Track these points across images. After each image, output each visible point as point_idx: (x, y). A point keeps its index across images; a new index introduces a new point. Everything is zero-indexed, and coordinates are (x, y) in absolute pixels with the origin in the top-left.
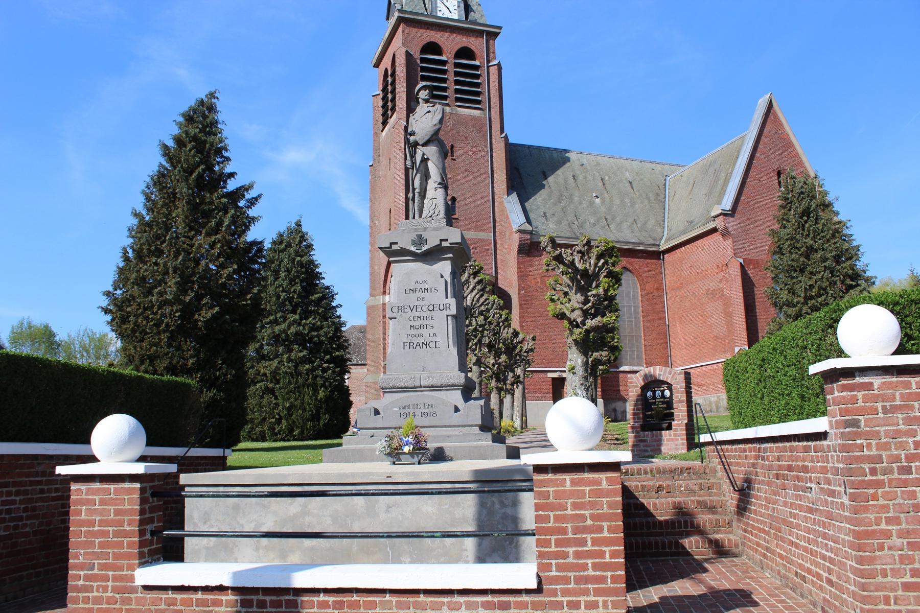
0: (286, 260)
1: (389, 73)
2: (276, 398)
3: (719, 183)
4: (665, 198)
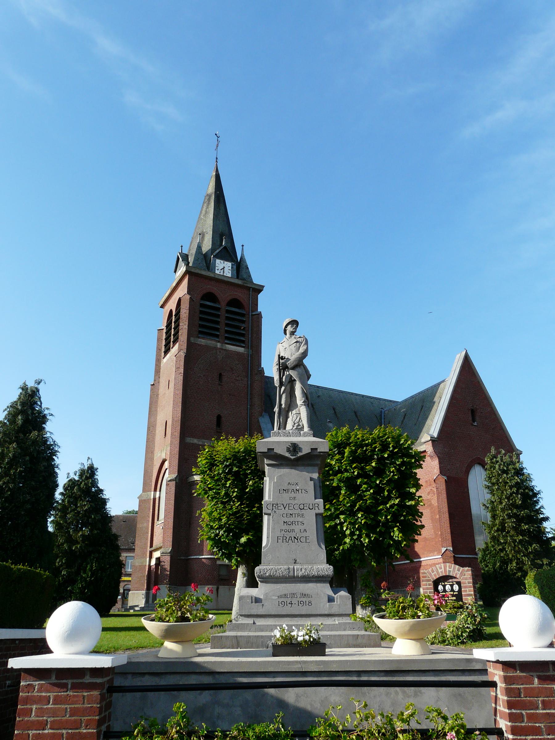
1: (174, 314)
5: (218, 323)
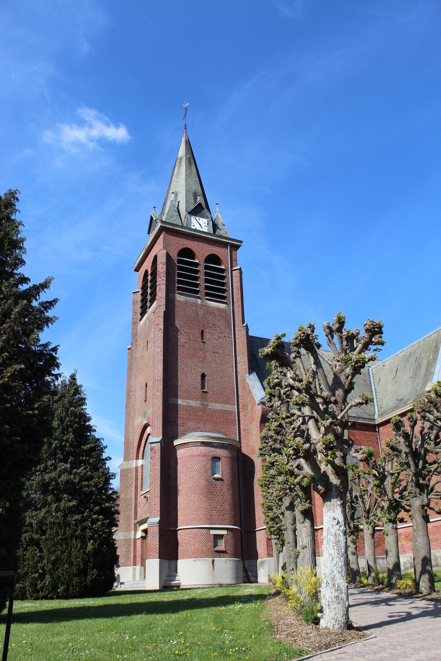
0: (60, 409)
1: (149, 273)
2: (41, 551)
3: (423, 367)
4: (371, 383)
5: (197, 279)
